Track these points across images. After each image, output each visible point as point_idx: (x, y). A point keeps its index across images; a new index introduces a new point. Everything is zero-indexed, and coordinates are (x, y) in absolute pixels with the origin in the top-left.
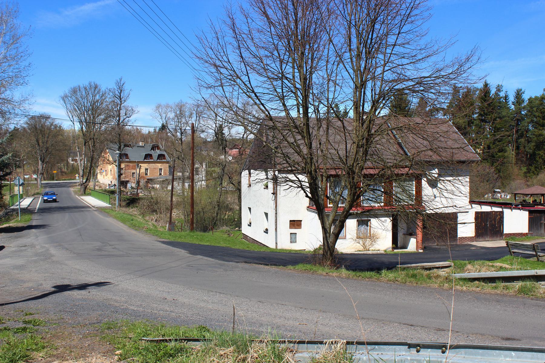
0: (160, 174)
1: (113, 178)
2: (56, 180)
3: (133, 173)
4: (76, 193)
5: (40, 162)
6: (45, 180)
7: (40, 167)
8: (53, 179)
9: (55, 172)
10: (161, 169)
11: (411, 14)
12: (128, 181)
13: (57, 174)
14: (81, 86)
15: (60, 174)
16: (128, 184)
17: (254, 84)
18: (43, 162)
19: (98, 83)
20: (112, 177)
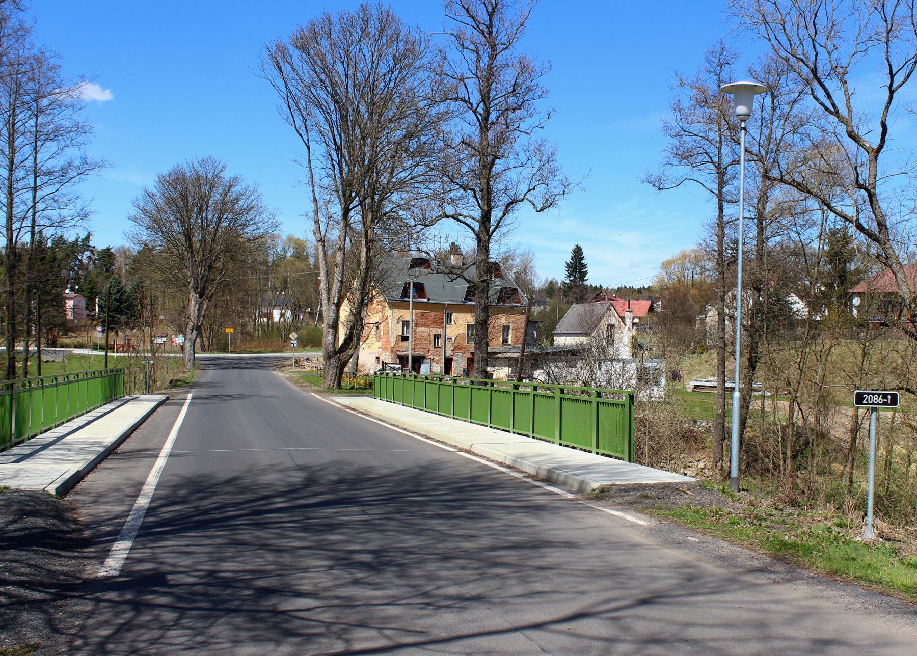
0: (505, 341)
1: (384, 349)
2: (232, 352)
3: (437, 337)
4: (310, 379)
5: (193, 297)
6: (203, 350)
7: (193, 310)
8: (224, 350)
9: (230, 330)
10: (506, 329)
11: (15, 162)
12: (423, 357)
13: (234, 338)
14: (286, 41)
15: (240, 336)
16: (423, 366)
17: (420, 167)
18: (201, 296)
19: (398, 12)
20: (379, 344)
